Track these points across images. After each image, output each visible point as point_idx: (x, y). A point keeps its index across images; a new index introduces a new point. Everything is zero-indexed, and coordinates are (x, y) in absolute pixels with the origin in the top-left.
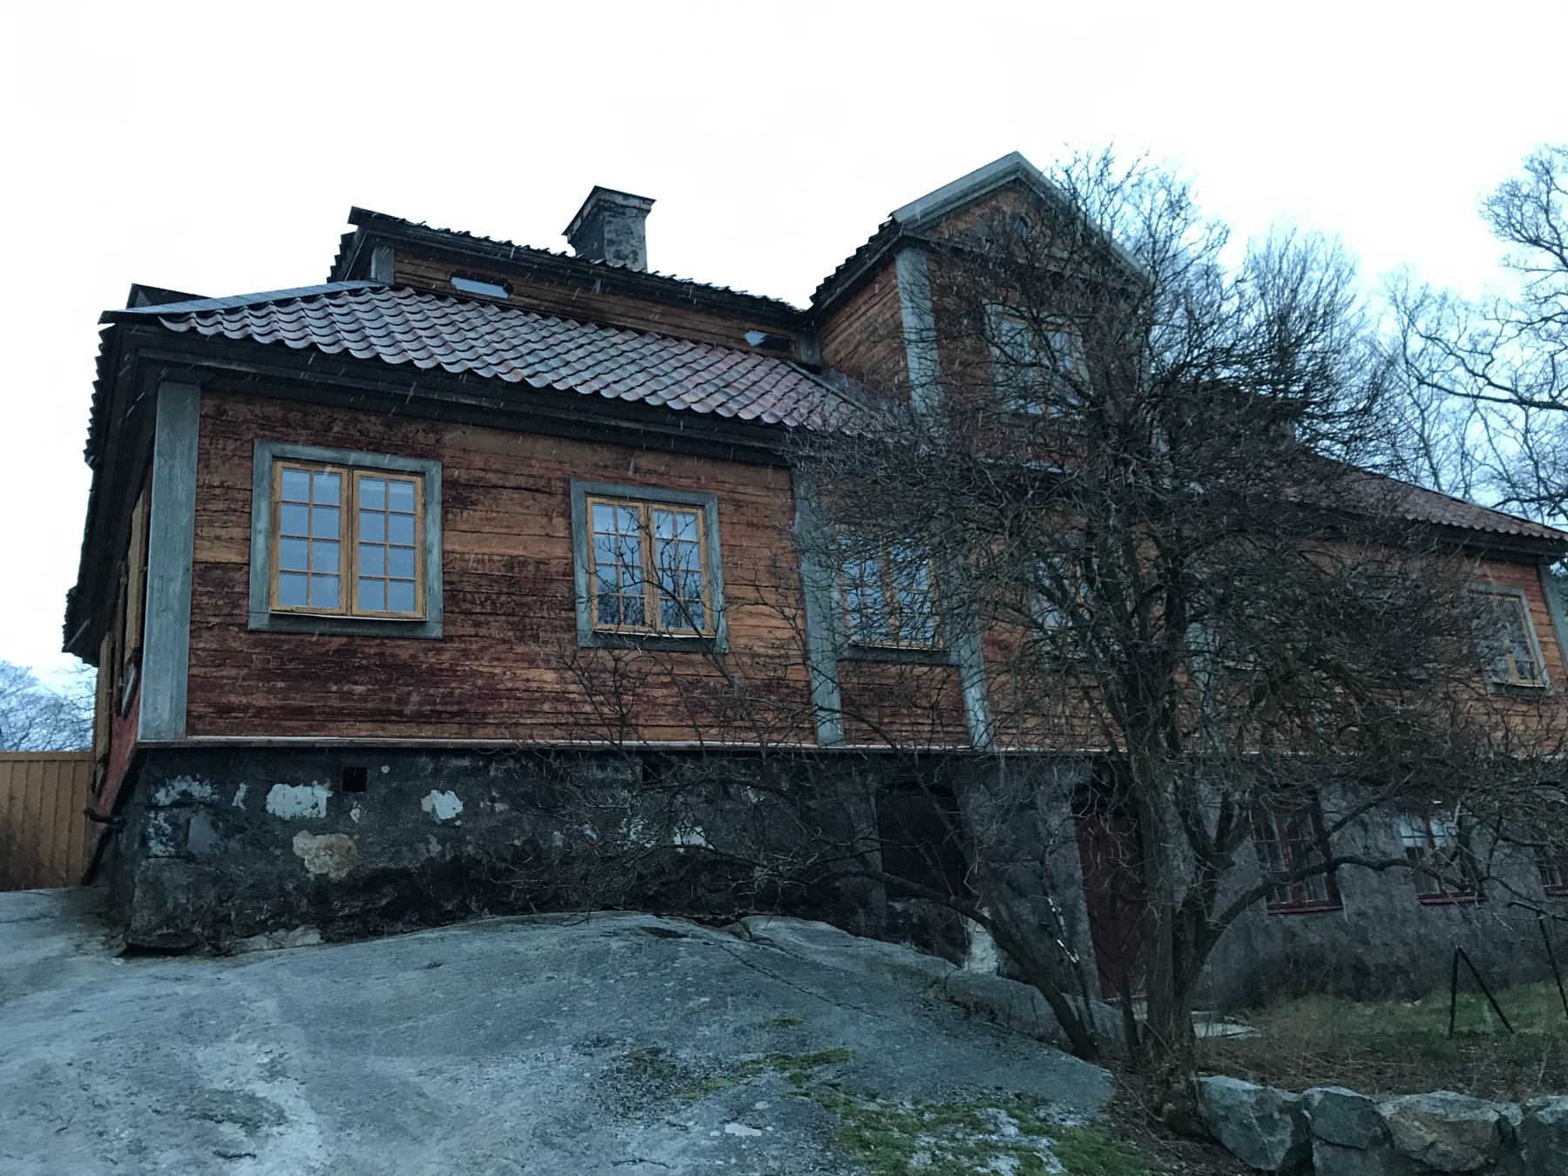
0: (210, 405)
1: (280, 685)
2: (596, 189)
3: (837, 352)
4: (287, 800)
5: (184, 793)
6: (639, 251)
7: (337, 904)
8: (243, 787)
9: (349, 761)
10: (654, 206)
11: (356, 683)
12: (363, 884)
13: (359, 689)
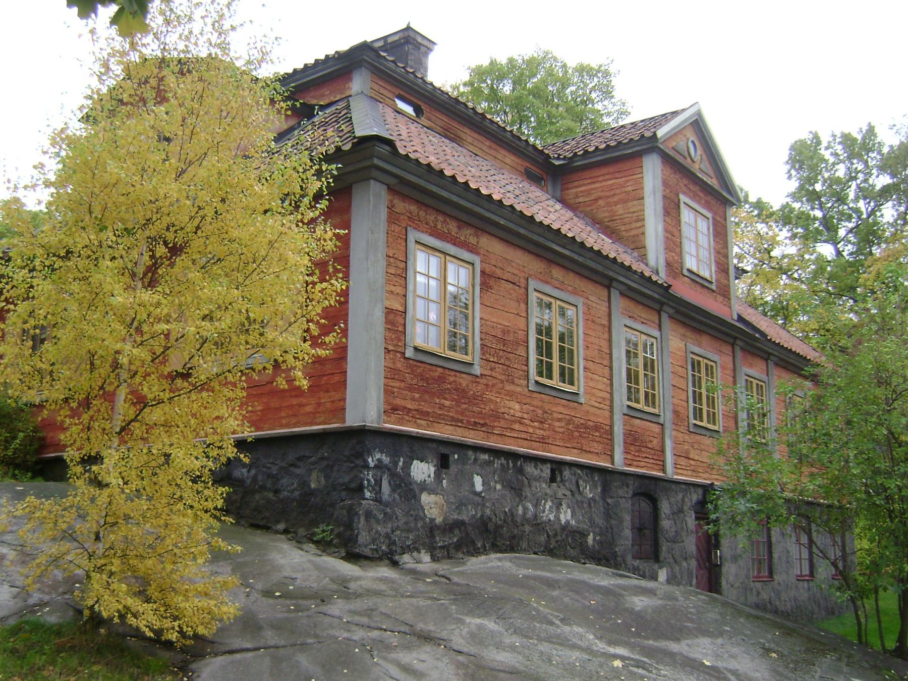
0: (390, 197)
1: (417, 396)
2: (409, 28)
3: (577, 197)
4: (422, 470)
5: (379, 460)
6: (421, 64)
7: (438, 539)
8: (402, 459)
9: (444, 450)
10: (436, 47)
11: (446, 399)
12: (450, 527)
13: (447, 403)
